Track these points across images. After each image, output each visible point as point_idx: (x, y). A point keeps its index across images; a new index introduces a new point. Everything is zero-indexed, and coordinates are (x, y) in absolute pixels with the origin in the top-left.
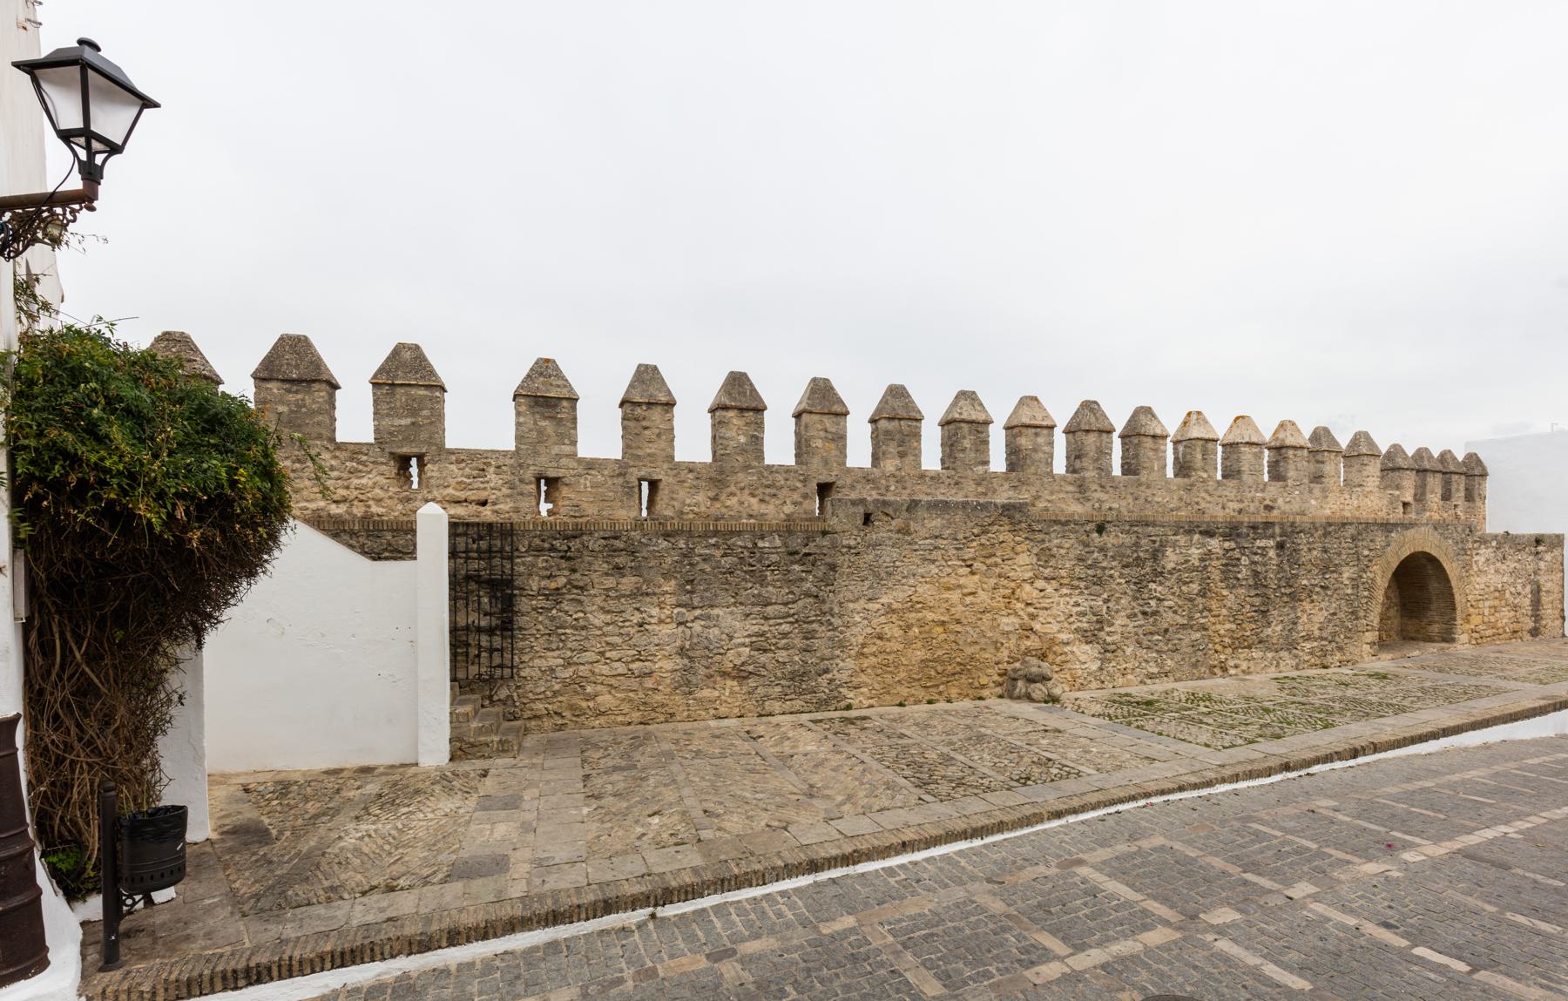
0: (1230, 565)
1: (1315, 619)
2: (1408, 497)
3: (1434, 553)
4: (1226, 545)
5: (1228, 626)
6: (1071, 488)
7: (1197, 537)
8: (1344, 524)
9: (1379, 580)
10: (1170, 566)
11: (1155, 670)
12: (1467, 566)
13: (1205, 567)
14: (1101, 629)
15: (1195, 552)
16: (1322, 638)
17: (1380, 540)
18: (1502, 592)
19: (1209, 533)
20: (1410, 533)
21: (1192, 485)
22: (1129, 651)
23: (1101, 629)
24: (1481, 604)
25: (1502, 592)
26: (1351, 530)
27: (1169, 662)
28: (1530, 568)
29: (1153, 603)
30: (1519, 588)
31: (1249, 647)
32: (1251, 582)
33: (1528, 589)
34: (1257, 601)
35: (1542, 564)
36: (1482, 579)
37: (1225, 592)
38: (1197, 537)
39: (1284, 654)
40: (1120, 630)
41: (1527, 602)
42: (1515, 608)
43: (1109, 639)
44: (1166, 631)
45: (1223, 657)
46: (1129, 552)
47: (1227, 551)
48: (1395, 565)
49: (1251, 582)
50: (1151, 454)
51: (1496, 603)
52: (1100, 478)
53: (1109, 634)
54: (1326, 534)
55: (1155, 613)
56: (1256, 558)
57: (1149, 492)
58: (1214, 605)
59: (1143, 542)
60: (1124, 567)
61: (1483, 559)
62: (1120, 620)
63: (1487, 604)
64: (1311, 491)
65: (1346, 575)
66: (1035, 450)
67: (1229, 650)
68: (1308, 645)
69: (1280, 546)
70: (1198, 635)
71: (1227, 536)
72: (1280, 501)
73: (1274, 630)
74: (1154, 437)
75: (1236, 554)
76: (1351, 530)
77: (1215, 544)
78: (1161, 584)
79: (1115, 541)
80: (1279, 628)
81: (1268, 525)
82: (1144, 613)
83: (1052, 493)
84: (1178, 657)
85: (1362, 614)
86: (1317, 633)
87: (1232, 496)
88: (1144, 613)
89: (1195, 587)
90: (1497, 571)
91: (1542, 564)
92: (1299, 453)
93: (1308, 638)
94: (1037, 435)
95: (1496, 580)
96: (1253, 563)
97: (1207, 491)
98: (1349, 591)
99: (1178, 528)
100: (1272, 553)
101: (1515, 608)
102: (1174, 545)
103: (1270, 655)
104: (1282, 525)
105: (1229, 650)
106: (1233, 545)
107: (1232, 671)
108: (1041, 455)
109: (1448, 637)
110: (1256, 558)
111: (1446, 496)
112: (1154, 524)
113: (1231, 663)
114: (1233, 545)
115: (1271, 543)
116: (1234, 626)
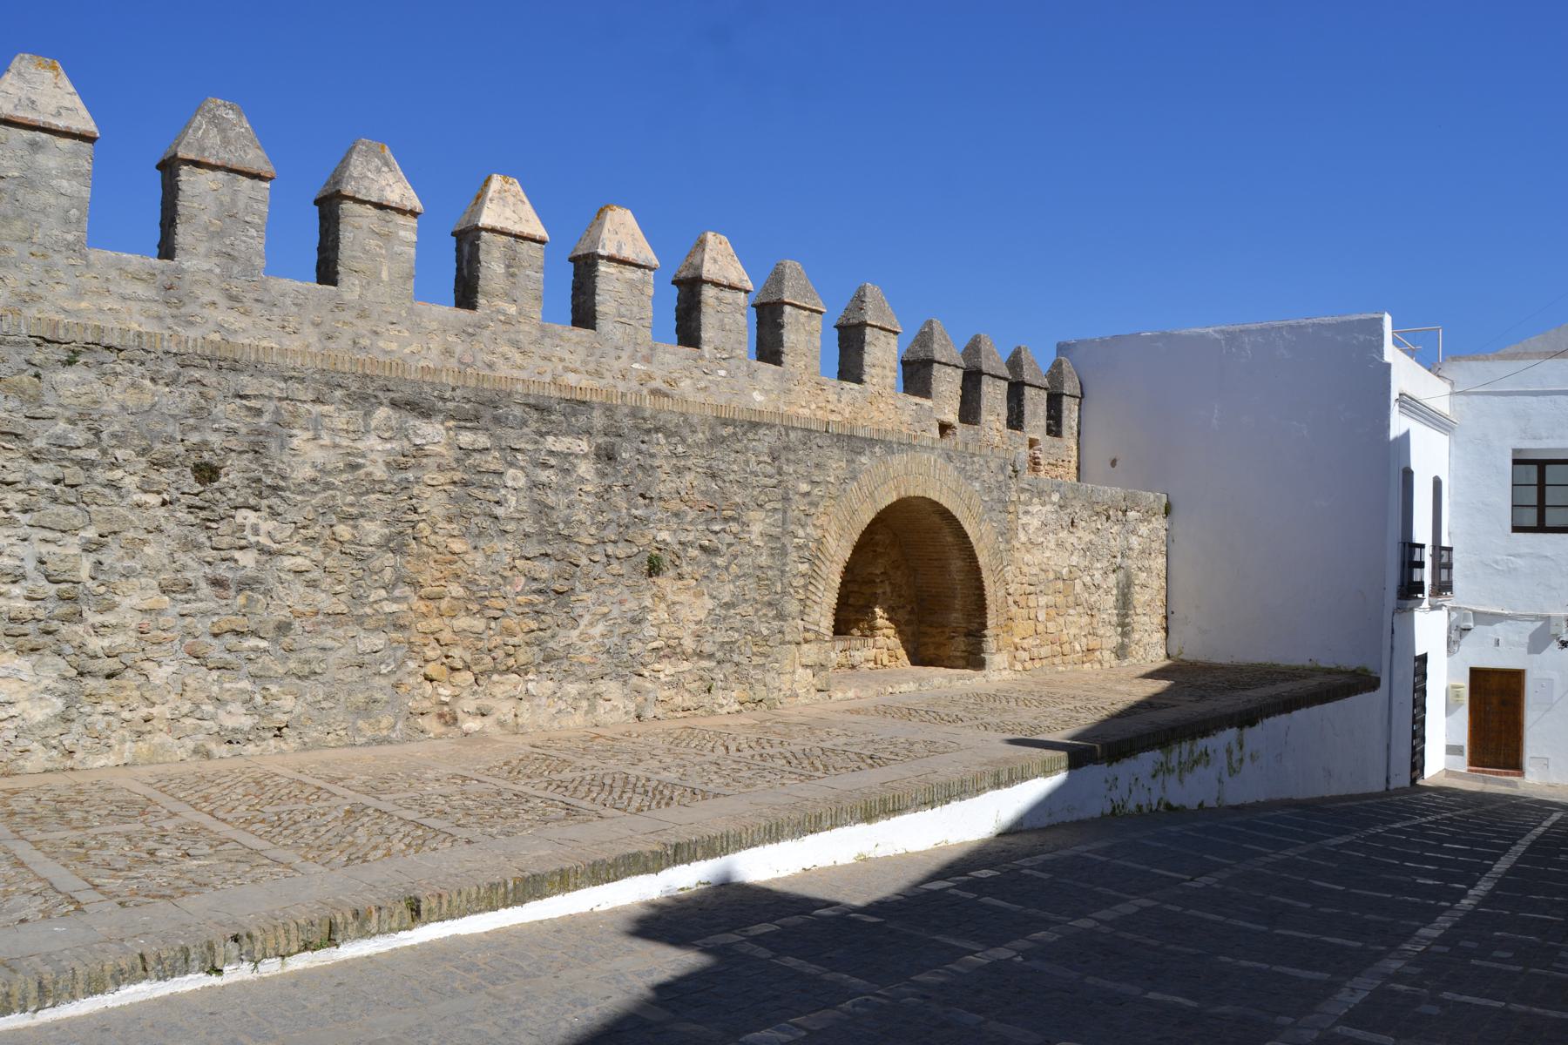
0: (471, 483)
1: (684, 613)
2: (951, 417)
3: (944, 501)
4: (466, 438)
5: (463, 622)
6: (140, 289)
7: (382, 413)
8: (755, 426)
9: (831, 543)
10: (304, 473)
11: (246, 722)
12: (1007, 533)
13: (405, 486)
14: (78, 617)
15: (376, 450)
16: (700, 655)
17: (836, 464)
18: (1069, 580)
19: (418, 408)
20: (898, 461)
21: (479, 326)
22: (160, 675)
23: (78, 617)
24: (1032, 601)
25: (1069, 580)
26: (767, 439)
27: (288, 702)
28: (1116, 545)
29: (247, 559)
30: (1098, 575)
31: (521, 671)
32: (529, 526)
33: (1112, 578)
34: (544, 569)
35: (1134, 540)
36: (1033, 558)
37: (457, 546)
38: (382, 413)
39: (610, 687)
40: (134, 620)
41: (1111, 600)
42: (1091, 611)
43: (95, 644)
44: (283, 628)
45: (445, 693)
46: (172, 429)
47: (468, 452)
48: (867, 517)
49: (529, 526)
50: (373, 243)
51: (1060, 600)
52: (227, 275)
53: (97, 630)
54: (715, 441)
55: (245, 585)
56: (544, 475)
57: (363, 326)
58: (428, 575)
59: (219, 409)
60: (156, 464)
61: (1036, 523)
62: (134, 598)
63: (1043, 600)
64: (752, 375)
65: (756, 528)
66: (27, 182)
67: (467, 677)
68: (667, 668)
69: (607, 456)
70: (378, 641)
71: (466, 419)
72: (685, 384)
73: (587, 633)
74: (380, 206)
75: (492, 461)
76: (767, 439)
77: (432, 433)
78: (274, 514)
79: (131, 399)
80: (600, 628)
81: (578, 405)
82: (217, 583)
83: (79, 294)
84: (314, 690)
85: (793, 607)
86: (689, 644)
87: (575, 360)
88: (217, 583)
89: (374, 531)
90: (1061, 545)
91: (1134, 540)
92: (728, 295)
93: (671, 651)
94: (34, 146)
95: (1062, 562)
96: (535, 485)
97: (515, 344)
98: (764, 560)
99: (328, 384)
100: (585, 469)
101: (1091, 611)
102: (316, 426)
103: (572, 689)
104: (609, 410)
105: (467, 677)
106: (483, 440)
107: (472, 725)
108: (47, 197)
109: (975, 661)
110: (544, 475)
111: (1015, 420)
112: (257, 369)
113: (469, 704)
114: (483, 440)
115: (584, 446)
116: (479, 624)
